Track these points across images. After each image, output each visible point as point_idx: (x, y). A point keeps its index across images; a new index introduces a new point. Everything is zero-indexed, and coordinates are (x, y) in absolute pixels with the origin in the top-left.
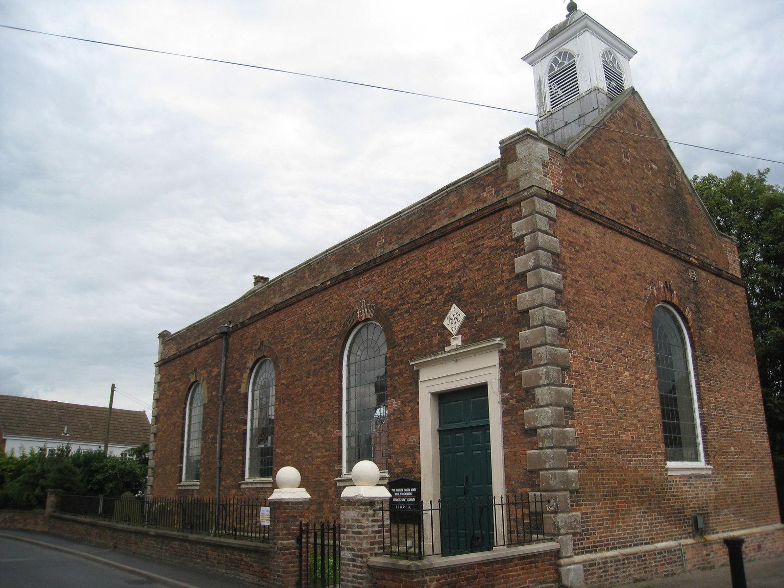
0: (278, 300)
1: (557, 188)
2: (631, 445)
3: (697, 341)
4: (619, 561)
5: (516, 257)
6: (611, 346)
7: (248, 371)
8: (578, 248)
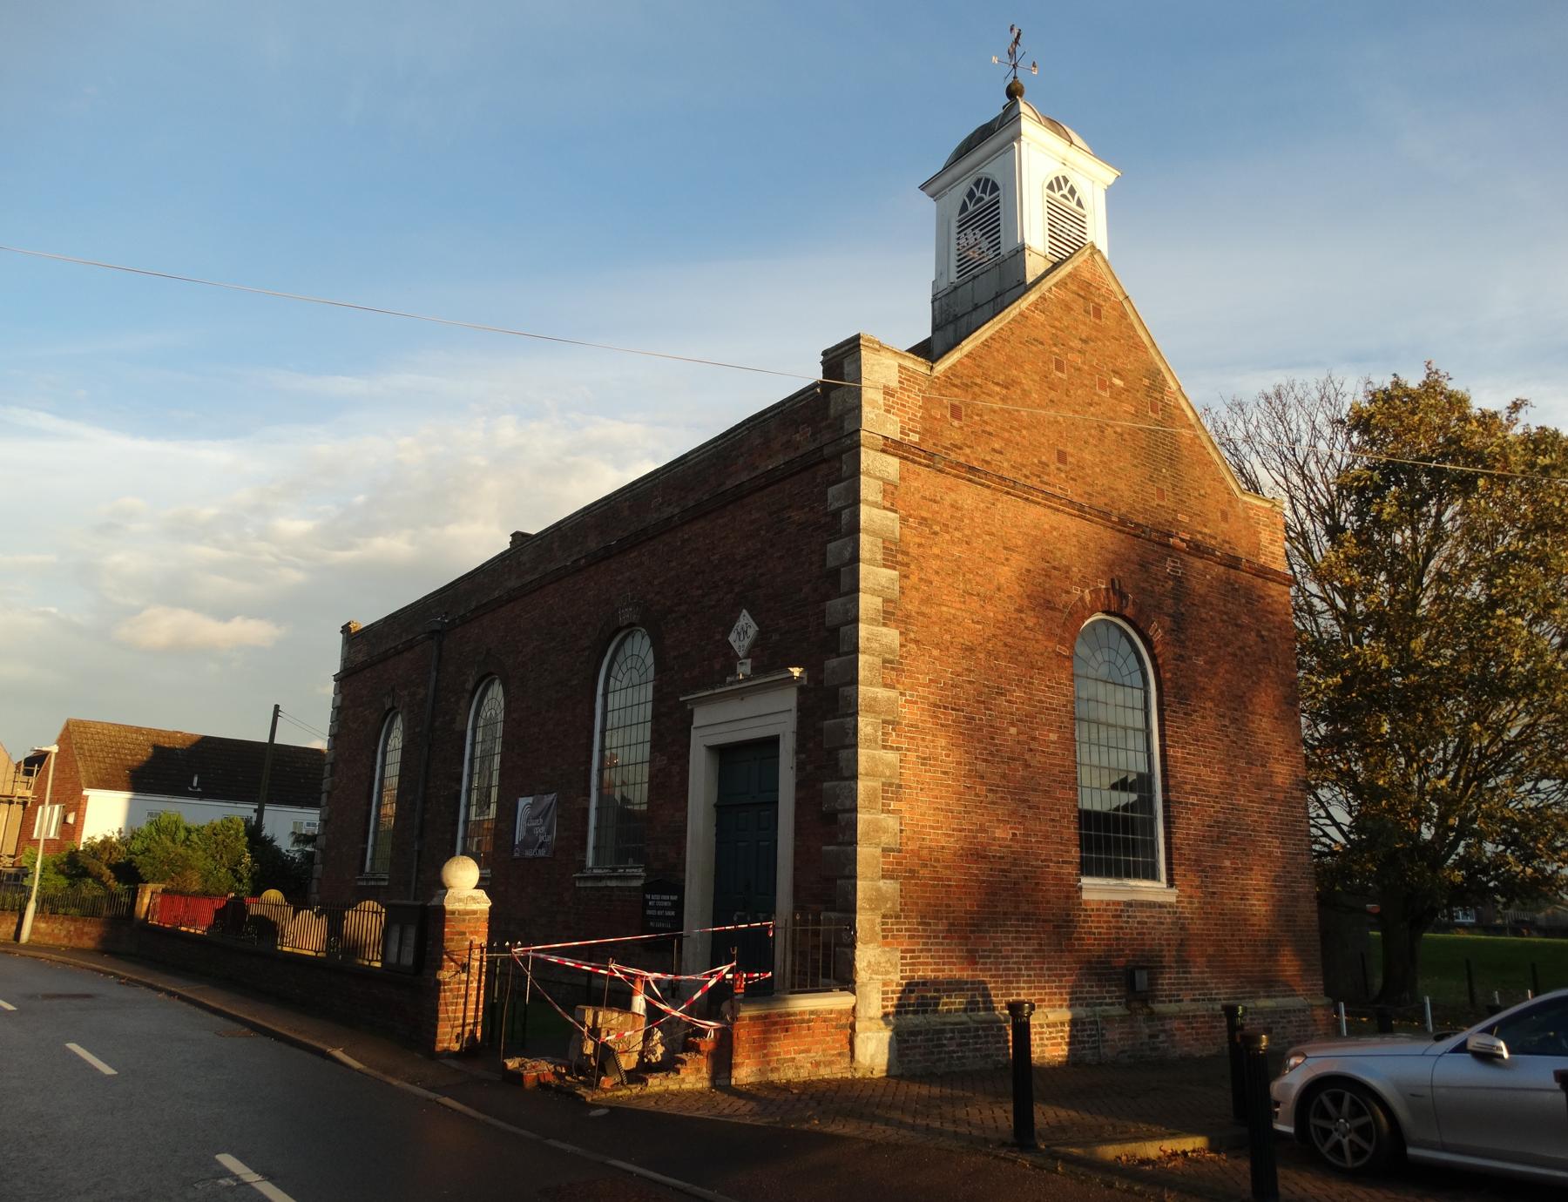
0: (513, 583)
1: (910, 430)
2: (1010, 847)
3: (1170, 679)
4: (968, 1030)
5: (830, 541)
6: (985, 686)
7: (467, 696)
8: (936, 528)
